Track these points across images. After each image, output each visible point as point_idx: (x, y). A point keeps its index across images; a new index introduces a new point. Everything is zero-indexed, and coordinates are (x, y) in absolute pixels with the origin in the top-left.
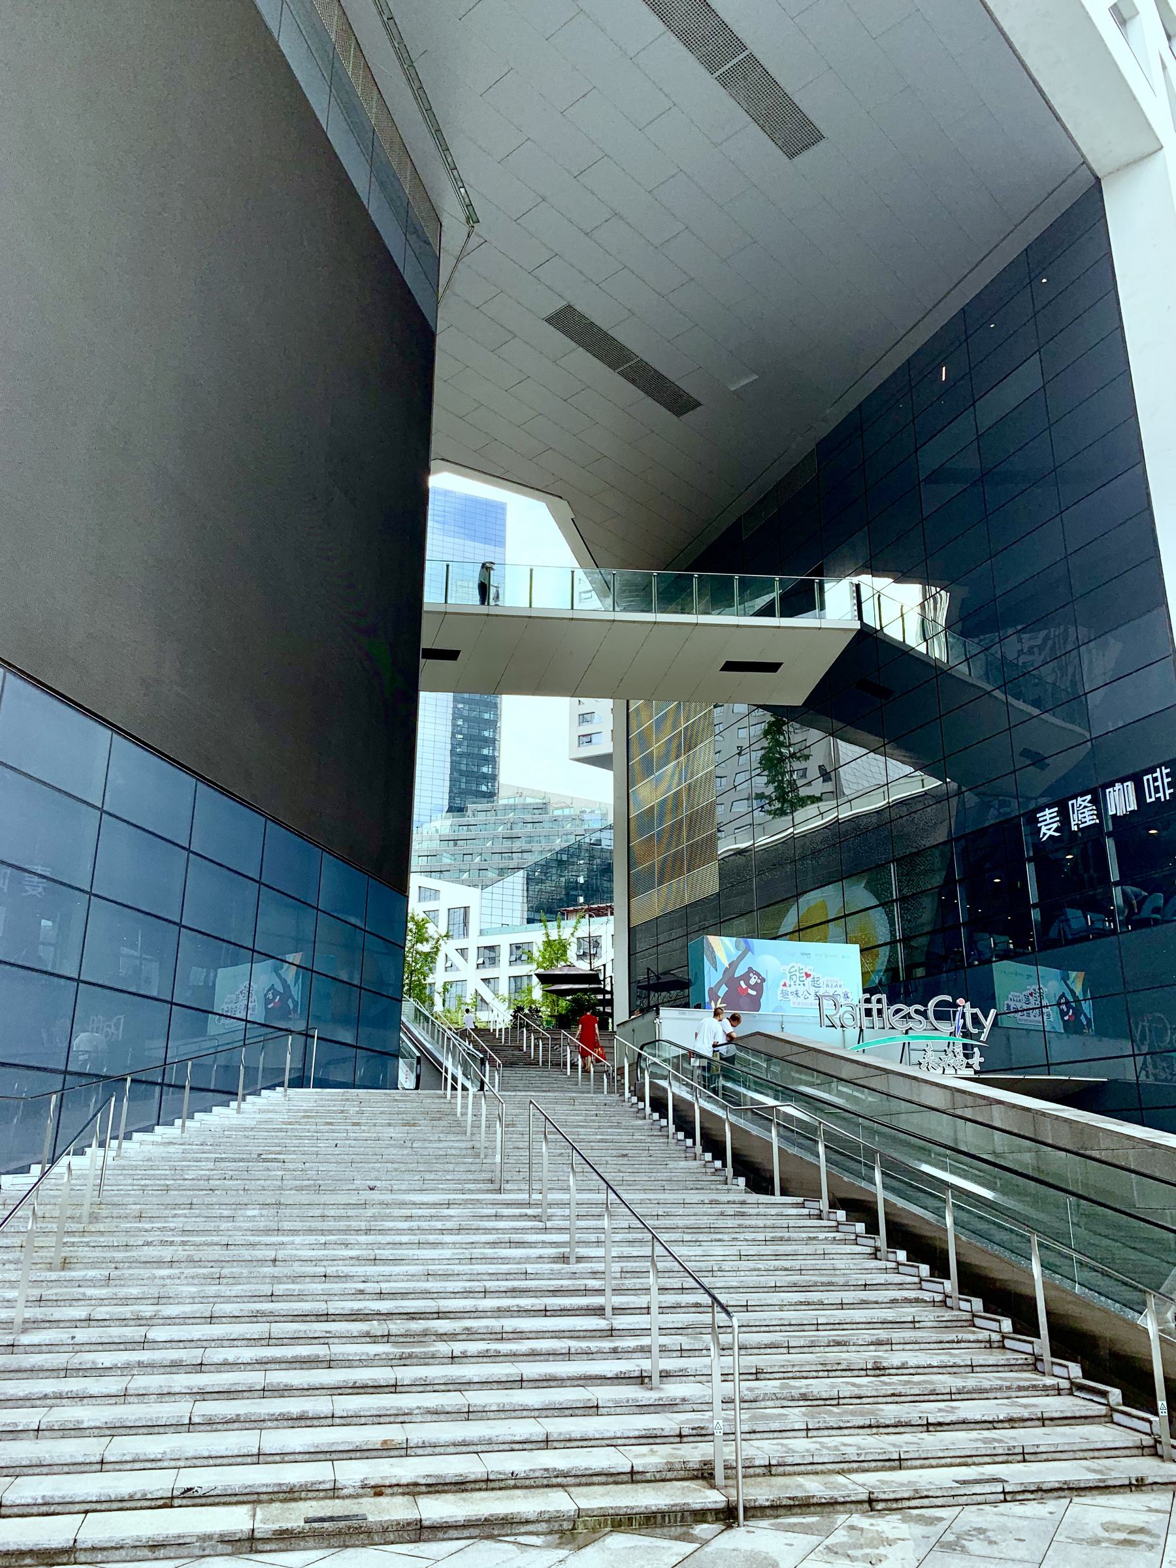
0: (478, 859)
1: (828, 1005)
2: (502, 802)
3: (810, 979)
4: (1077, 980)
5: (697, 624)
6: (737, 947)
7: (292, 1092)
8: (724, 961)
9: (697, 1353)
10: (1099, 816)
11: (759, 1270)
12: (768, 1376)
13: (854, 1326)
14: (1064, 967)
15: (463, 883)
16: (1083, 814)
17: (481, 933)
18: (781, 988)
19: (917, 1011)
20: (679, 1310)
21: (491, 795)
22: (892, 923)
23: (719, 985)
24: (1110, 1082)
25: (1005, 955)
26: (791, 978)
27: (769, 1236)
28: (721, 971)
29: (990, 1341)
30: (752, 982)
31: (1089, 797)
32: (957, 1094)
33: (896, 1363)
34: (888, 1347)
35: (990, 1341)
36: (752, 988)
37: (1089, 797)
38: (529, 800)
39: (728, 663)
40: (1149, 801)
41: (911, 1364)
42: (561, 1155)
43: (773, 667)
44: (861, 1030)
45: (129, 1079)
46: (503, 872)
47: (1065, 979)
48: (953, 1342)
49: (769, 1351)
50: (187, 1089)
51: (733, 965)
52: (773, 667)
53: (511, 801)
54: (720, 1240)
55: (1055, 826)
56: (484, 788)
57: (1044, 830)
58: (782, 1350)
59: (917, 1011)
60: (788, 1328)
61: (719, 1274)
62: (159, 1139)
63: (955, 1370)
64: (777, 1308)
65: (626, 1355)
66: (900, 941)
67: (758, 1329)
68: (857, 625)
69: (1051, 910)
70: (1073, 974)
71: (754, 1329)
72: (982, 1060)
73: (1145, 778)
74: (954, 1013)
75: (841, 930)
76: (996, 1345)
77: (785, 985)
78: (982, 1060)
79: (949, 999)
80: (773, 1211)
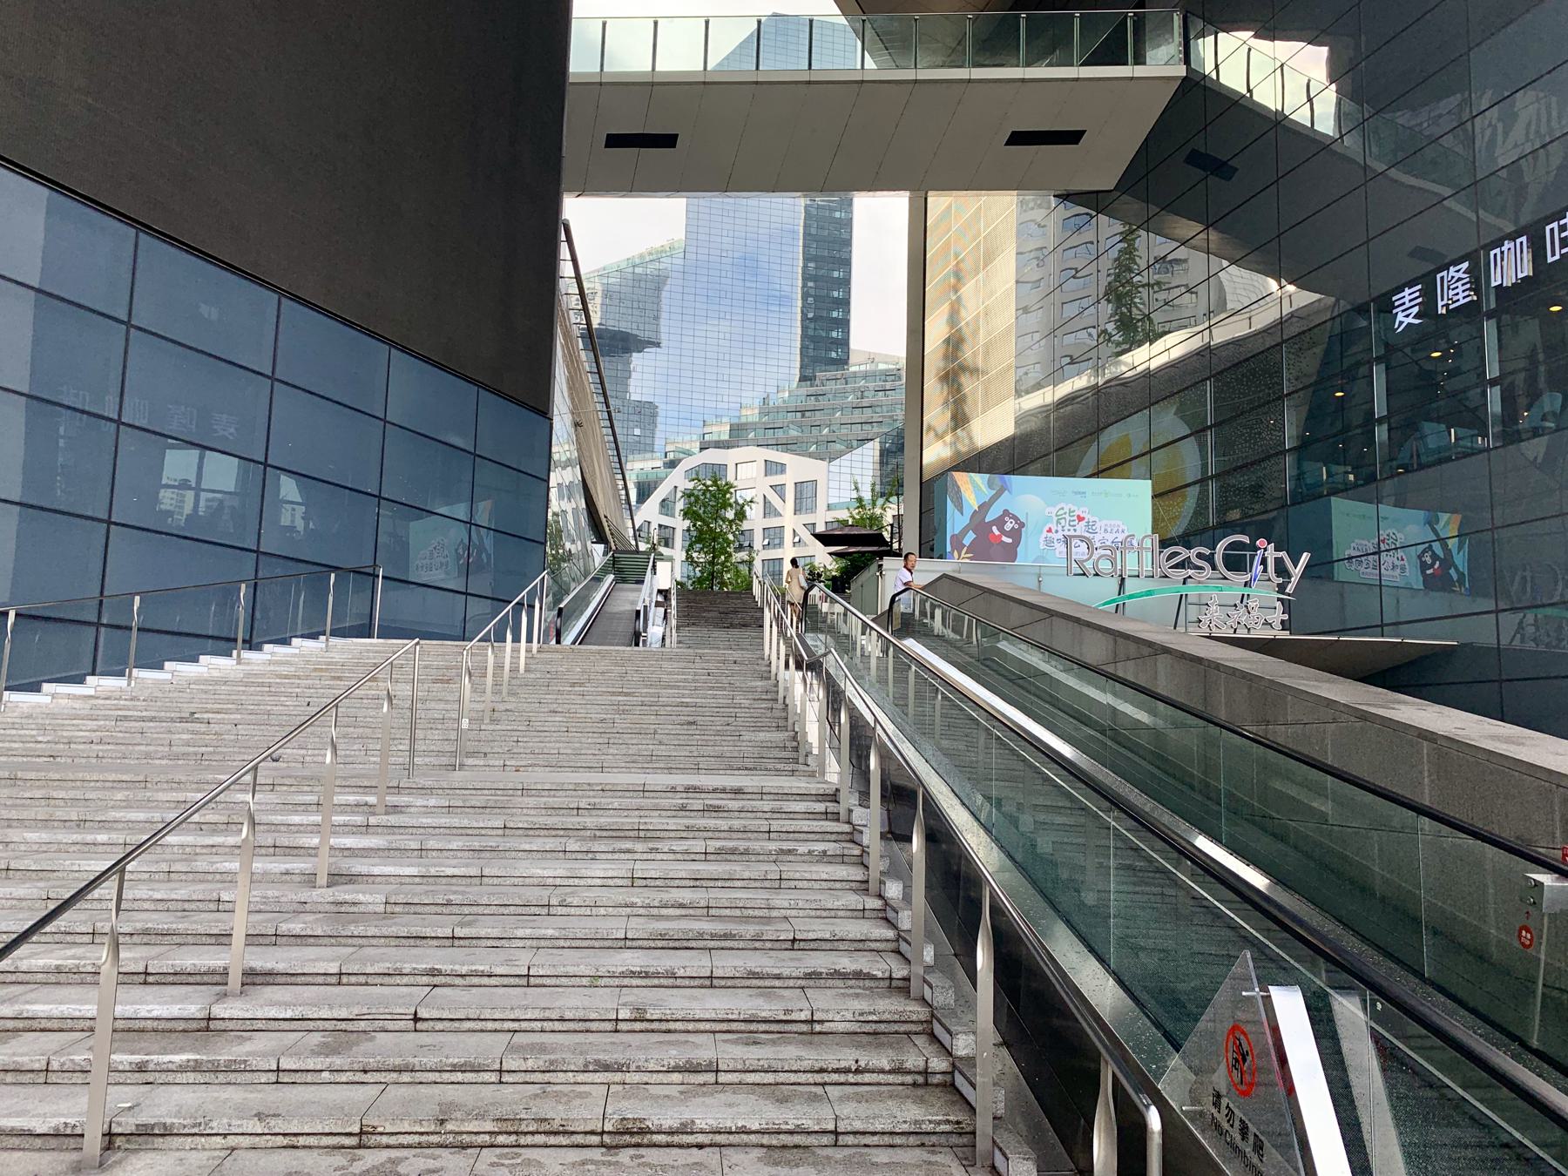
0: (826, 431)
1: (1080, 550)
2: (852, 369)
3: (1083, 523)
4: (1448, 524)
5: (969, 81)
6: (990, 485)
7: (334, 641)
8: (972, 501)
9: (309, 1077)
10: (1476, 290)
11: (632, 905)
12: (385, 1140)
13: (691, 1026)
14: (1433, 510)
15: (810, 456)
16: (1455, 289)
17: (829, 508)
18: (1045, 534)
19: (1199, 556)
20: (398, 980)
21: (843, 362)
22: (1204, 457)
23: (964, 532)
24: (1462, 646)
25: (1343, 490)
26: (1058, 522)
27: (713, 845)
28: (968, 513)
29: (925, 1072)
30: (1008, 527)
31: (1465, 265)
32: (1120, 640)
33: (669, 1122)
34: (710, 1078)
35: (925, 1072)
36: (1007, 534)
37: (1465, 265)
38: (882, 367)
39: (1014, 133)
40: (1550, 260)
41: (701, 1124)
42: (602, 721)
43: (1073, 137)
44: (1123, 580)
45: (12, 615)
46: (863, 441)
47: (1431, 523)
48: (847, 1071)
49: (459, 1077)
50: (135, 630)
51: (985, 507)
52: (1073, 137)
53: (863, 368)
54: (629, 851)
55: (1416, 310)
56: (834, 355)
57: (1400, 317)
58: (487, 1077)
59: (1199, 556)
60: (558, 1026)
61: (561, 911)
62: (91, 692)
63: (797, 1139)
64: (585, 981)
65: (163, 1077)
66: (1212, 477)
67: (497, 1025)
68: (1181, 71)
69: (1405, 425)
70: (1444, 517)
71: (490, 1025)
72: (1286, 617)
73: (1548, 228)
74: (1252, 558)
75: (1143, 470)
76: (937, 1079)
77: (1050, 531)
78: (1286, 617)
79: (1246, 539)
80: (767, 805)
